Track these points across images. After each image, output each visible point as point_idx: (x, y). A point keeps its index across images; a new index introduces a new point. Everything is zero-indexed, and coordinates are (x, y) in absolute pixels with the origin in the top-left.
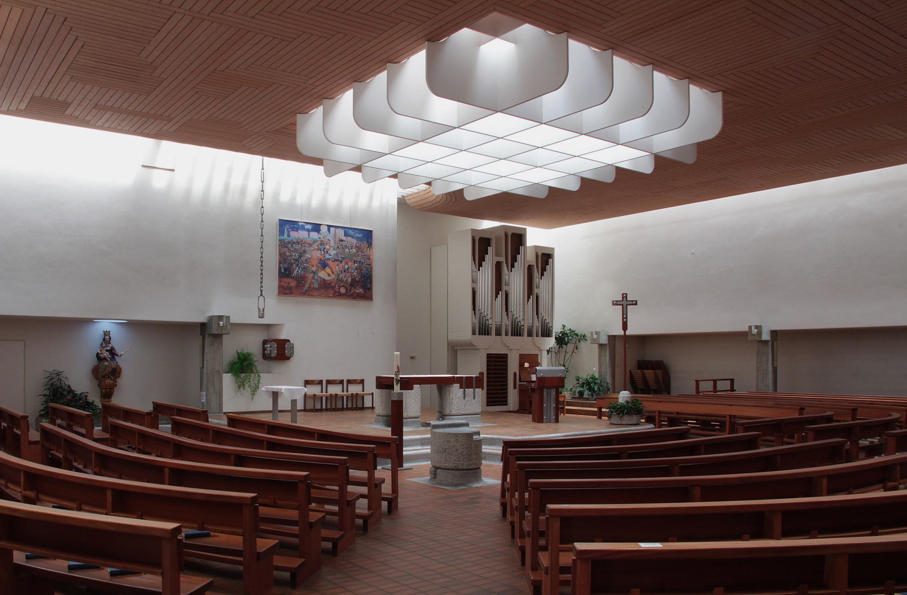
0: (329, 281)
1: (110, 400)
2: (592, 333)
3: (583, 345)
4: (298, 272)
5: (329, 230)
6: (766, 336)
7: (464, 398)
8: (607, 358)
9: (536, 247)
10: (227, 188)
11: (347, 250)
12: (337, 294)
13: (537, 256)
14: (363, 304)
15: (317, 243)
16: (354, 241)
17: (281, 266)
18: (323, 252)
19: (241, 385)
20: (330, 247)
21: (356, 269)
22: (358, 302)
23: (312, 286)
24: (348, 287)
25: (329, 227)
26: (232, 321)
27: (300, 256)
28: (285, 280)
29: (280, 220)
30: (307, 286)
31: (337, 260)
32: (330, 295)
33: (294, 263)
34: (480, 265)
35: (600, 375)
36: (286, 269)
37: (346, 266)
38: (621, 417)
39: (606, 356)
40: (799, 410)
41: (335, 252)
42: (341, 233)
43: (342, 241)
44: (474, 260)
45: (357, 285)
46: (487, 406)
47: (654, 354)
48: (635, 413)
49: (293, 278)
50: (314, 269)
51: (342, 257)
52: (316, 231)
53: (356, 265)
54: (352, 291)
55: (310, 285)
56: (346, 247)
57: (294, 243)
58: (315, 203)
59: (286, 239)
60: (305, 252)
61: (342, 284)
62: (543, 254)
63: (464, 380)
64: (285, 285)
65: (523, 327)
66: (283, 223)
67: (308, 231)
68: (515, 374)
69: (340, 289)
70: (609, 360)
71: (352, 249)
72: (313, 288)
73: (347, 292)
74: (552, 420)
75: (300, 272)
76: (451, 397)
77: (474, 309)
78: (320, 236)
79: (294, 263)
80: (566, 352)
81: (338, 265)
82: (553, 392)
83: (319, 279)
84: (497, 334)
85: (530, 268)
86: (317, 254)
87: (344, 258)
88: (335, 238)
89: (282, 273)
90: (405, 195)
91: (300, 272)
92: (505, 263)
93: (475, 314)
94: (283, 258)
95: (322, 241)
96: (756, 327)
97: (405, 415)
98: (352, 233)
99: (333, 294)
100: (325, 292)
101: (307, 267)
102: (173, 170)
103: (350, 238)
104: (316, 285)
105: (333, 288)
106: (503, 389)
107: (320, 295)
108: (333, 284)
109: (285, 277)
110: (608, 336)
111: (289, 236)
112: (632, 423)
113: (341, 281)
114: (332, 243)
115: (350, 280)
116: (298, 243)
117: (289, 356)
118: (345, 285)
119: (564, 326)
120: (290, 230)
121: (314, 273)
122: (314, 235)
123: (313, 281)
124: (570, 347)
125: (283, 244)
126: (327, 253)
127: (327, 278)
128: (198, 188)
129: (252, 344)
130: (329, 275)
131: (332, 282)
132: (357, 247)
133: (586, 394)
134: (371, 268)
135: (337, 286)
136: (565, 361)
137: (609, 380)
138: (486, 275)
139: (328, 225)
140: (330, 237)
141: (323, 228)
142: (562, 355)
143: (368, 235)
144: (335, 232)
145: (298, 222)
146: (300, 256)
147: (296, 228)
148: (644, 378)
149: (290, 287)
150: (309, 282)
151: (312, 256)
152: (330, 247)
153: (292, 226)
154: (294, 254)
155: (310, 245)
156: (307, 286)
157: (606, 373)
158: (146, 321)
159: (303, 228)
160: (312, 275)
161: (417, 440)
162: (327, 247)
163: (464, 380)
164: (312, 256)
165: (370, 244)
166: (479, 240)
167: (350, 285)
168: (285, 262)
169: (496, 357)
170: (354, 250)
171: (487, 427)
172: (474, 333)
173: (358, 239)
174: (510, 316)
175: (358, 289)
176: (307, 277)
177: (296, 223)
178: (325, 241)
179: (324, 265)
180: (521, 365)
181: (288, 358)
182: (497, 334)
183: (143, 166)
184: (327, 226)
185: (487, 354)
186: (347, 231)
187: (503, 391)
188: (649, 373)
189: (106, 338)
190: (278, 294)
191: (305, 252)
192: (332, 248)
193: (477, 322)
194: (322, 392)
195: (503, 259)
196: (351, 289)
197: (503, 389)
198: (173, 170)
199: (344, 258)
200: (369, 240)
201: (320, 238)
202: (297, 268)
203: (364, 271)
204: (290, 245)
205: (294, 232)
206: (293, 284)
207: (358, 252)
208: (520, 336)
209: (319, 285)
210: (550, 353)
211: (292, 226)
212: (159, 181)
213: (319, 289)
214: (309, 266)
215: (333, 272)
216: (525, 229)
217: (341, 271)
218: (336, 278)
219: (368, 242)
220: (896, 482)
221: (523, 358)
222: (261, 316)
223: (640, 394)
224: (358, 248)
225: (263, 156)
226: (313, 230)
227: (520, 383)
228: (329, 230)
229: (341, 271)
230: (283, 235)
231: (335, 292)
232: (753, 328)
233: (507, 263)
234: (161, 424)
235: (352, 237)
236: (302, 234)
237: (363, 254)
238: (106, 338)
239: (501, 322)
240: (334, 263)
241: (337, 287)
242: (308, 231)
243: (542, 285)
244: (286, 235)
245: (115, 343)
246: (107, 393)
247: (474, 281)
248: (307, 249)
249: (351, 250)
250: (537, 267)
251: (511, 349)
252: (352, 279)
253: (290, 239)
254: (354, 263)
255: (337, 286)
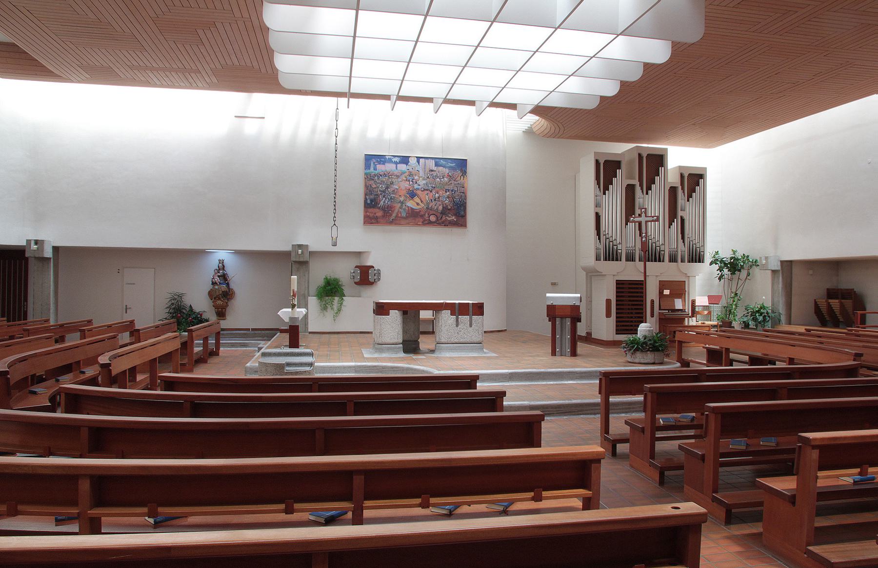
0: (418, 210)
1: (224, 318)
2: (761, 258)
3: (756, 271)
4: (384, 202)
5: (418, 162)
6: (48, 253)
7: (457, 325)
8: (780, 285)
9: (680, 167)
10: (314, 131)
11: (438, 179)
12: (426, 222)
13: (682, 176)
14: (456, 230)
15: (405, 174)
16: (447, 171)
17: (367, 197)
18: (411, 183)
19: (324, 308)
20: (420, 177)
21: (448, 197)
22: (450, 229)
23: (400, 215)
24: (439, 215)
25: (418, 158)
26: (311, 249)
27: (387, 188)
28: (371, 210)
29: (366, 155)
30: (394, 215)
31: (427, 190)
32: (419, 223)
33: (381, 194)
34: (606, 188)
35: (773, 304)
36: (372, 201)
37: (437, 195)
38: (632, 354)
39: (779, 284)
40: (855, 356)
41: (424, 182)
42: (431, 164)
43: (432, 171)
44: (598, 183)
45: (449, 213)
46: (616, 334)
47: (848, 281)
48: (651, 349)
49: (379, 208)
50: (402, 199)
51: (432, 187)
52: (404, 163)
53: (448, 193)
54: (444, 219)
55: (397, 214)
56: (437, 176)
57: (381, 175)
58: (404, 137)
59: (372, 172)
60: (392, 183)
61: (431, 212)
62: (691, 175)
63: (457, 307)
64: (371, 215)
65: (663, 252)
66: (369, 158)
67: (396, 163)
68: (652, 301)
69: (429, 217)
70: (782, 288)
71: (443, 178)
72: (401, 217)
73: (437, 219)
74: (567, 353)
75: (386, 202)
76: (440, 324)
77: (598, 234)
78: (408, 167)
79: (381, 194)
80: (739, 278)
81: (427, 194)
82: (568, 322)
83: (407, 209)
84: (627, 260)
85: (673, 191)
86: (405, 185)
87: (435, 188)
88: (425, 168)
89: (368, 204)
90: (532, 123)
91: (386, 202)
92: (680, 188)
93: (599, 239)
94: (368, 190)
95: (410, 172)
96: (36, 242)
97: (612, 340)
98: (444, 163)
99: (422, 222)
100: (414, 221)
101: (394, 197)
102: (264, 118)
103: (441, 168)
104: (404, 215)
105: (422, 216)
106: (639, 317)
107: (408, 224)
108: (422, 213)
109: (371, 208)
110: (781, 261)
111: (375, 169)
112: (646, 361)
113: (431, 209)
114: (421, 174)
115: (441, 208)
116: (385, 175)
117: (373, 281)
118: (434, 213)
119: (734, 252)
120: (376, 163)
121: (402, 203)
122: (402, 167)
123: (400, 210)
124: (744, 273)
125: (368, 177)
126: (416, 183)
127: (415, 207)
128: (286, 133)
129: (344, 271)
130: (418, 204)
131: (420, 211)
132: (449, 176)
133: (752, 324)
134: (466, 196)
135: (427, 214)
136: (738, 288)
137: (781, 309)
138: (615, 200)
139: (416, 157)
140: (420, 168)
141: (411, 160)
142: (734, 282)
143: (462, 164)
144: (425, 163)
145: (385, 156)
146: (387, 188)
147: (383, 161)
148: (829, 306)
149: (376, 216)
150: (396, 211)
151: (399, 187)
152: (420, 177)
153: (379, 160)
154: (380, 186)
155: (398, 177)
156: (394, 215)
157: (779, 302)
158: (257, 251)
159: (390, 161)
160: (399, 205)
161: (350, 367)
162: (416, 178)
163: (457, 307)
164: (399, 187)
165: (464, 173)
166: (604, 164)
167: (441, 213)
168: (371, 194)
169: (630, 284)
170: (446, 179)
171: (474, 357)
172: (598, 258)
173: (450, 168)
174: (603, 238)
175: (450, 217)
176: (395, 207)
177: (382, 157)
178: (413, 172)
179: (412, 195)
180: (661, 293)
181: (372, 284)
182: (627, 260)
183: (236, 117)
184: (416, 158)
185: (616, 280)
186: (438, 161)
187: (640, 320)
188: (835, 303)
189: (222, 266)
190: (364, 223)
191: (392, 184)
192: (421, 178)
193: (601, 247)
194: (433, 316)
195: (636, 182)
196: (442, 217)
197: (639, 317)
198: (264, 118)
199: (435, 188)
200: (463, 169)
201: (408, 170)
202: (384, 199)
203: (457, 199)
204: (376, 178)
205: (381, 165)
206: (379, 213)
207: (450, 181)
208: (660, 261)
209: (407, 214)
210: (722, 280)
211: (379, 160)
212: (250, 128)
213: (406, 218)
214: (397, 196)
215: (422, 201)
216: (666, 150)
217: (431, 200)
218: (425, 207)
219: (461, 171)
220: (591, 491)
221: (663, 285)
222: (335, 245)
223: (831, 328)
224: (451, 177)
225: (337, 97)
226: (400, 162)
227: (660, 311)
228: (418, 162)
229: (431, 200)
230: (369, 169)
231: (425, 220)
232: (33, 243)
233: (641, 185)
234: (210, 340)
235: (444, 167)
236: (390, 167)
237: (455, 182)
238: (222, 266)
239: (635, 246)
240: (422, 192)
241: (427, 215)
242: (396, 163)
243: (687, 210)
244: (373, 169)
245: (230, 271)
246: (221, 314)
247: (597, 205)
248: (394, 180)
249: (442, 180)
250: (683, 189)
251: (689, 276)
252: (443, 207)
253: (376, 172)
254: (446, 192)
255: (427, 214)
